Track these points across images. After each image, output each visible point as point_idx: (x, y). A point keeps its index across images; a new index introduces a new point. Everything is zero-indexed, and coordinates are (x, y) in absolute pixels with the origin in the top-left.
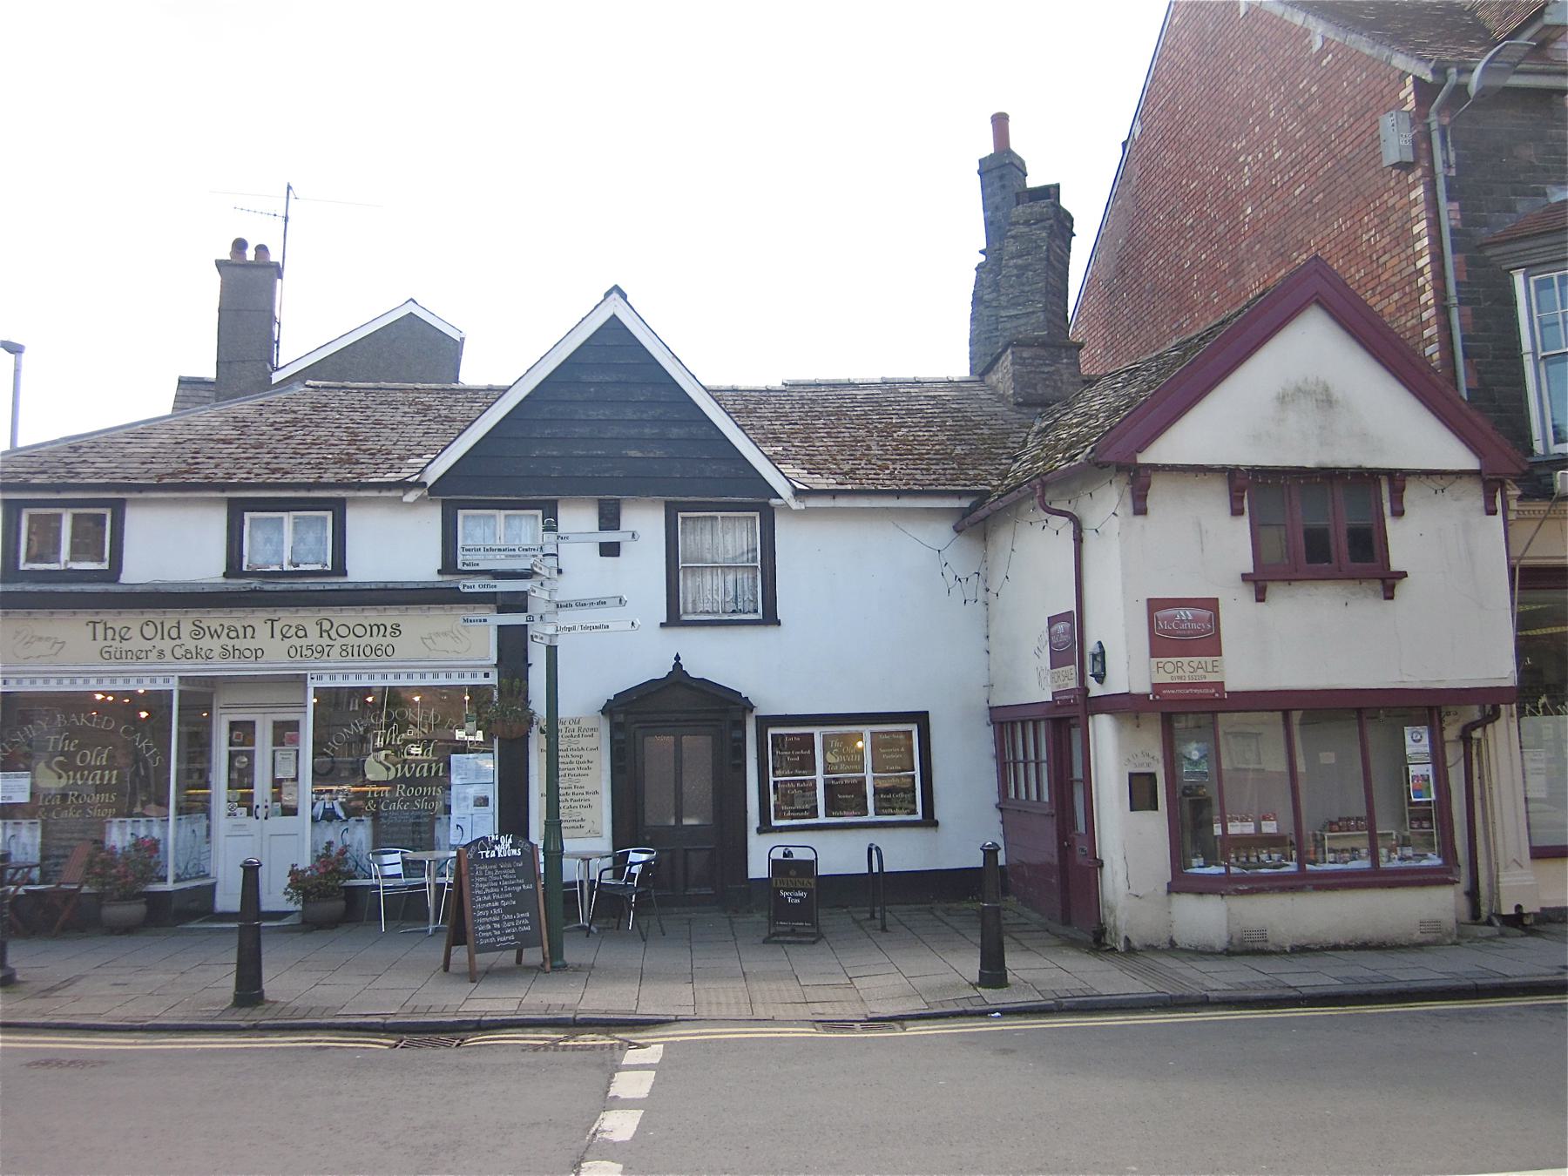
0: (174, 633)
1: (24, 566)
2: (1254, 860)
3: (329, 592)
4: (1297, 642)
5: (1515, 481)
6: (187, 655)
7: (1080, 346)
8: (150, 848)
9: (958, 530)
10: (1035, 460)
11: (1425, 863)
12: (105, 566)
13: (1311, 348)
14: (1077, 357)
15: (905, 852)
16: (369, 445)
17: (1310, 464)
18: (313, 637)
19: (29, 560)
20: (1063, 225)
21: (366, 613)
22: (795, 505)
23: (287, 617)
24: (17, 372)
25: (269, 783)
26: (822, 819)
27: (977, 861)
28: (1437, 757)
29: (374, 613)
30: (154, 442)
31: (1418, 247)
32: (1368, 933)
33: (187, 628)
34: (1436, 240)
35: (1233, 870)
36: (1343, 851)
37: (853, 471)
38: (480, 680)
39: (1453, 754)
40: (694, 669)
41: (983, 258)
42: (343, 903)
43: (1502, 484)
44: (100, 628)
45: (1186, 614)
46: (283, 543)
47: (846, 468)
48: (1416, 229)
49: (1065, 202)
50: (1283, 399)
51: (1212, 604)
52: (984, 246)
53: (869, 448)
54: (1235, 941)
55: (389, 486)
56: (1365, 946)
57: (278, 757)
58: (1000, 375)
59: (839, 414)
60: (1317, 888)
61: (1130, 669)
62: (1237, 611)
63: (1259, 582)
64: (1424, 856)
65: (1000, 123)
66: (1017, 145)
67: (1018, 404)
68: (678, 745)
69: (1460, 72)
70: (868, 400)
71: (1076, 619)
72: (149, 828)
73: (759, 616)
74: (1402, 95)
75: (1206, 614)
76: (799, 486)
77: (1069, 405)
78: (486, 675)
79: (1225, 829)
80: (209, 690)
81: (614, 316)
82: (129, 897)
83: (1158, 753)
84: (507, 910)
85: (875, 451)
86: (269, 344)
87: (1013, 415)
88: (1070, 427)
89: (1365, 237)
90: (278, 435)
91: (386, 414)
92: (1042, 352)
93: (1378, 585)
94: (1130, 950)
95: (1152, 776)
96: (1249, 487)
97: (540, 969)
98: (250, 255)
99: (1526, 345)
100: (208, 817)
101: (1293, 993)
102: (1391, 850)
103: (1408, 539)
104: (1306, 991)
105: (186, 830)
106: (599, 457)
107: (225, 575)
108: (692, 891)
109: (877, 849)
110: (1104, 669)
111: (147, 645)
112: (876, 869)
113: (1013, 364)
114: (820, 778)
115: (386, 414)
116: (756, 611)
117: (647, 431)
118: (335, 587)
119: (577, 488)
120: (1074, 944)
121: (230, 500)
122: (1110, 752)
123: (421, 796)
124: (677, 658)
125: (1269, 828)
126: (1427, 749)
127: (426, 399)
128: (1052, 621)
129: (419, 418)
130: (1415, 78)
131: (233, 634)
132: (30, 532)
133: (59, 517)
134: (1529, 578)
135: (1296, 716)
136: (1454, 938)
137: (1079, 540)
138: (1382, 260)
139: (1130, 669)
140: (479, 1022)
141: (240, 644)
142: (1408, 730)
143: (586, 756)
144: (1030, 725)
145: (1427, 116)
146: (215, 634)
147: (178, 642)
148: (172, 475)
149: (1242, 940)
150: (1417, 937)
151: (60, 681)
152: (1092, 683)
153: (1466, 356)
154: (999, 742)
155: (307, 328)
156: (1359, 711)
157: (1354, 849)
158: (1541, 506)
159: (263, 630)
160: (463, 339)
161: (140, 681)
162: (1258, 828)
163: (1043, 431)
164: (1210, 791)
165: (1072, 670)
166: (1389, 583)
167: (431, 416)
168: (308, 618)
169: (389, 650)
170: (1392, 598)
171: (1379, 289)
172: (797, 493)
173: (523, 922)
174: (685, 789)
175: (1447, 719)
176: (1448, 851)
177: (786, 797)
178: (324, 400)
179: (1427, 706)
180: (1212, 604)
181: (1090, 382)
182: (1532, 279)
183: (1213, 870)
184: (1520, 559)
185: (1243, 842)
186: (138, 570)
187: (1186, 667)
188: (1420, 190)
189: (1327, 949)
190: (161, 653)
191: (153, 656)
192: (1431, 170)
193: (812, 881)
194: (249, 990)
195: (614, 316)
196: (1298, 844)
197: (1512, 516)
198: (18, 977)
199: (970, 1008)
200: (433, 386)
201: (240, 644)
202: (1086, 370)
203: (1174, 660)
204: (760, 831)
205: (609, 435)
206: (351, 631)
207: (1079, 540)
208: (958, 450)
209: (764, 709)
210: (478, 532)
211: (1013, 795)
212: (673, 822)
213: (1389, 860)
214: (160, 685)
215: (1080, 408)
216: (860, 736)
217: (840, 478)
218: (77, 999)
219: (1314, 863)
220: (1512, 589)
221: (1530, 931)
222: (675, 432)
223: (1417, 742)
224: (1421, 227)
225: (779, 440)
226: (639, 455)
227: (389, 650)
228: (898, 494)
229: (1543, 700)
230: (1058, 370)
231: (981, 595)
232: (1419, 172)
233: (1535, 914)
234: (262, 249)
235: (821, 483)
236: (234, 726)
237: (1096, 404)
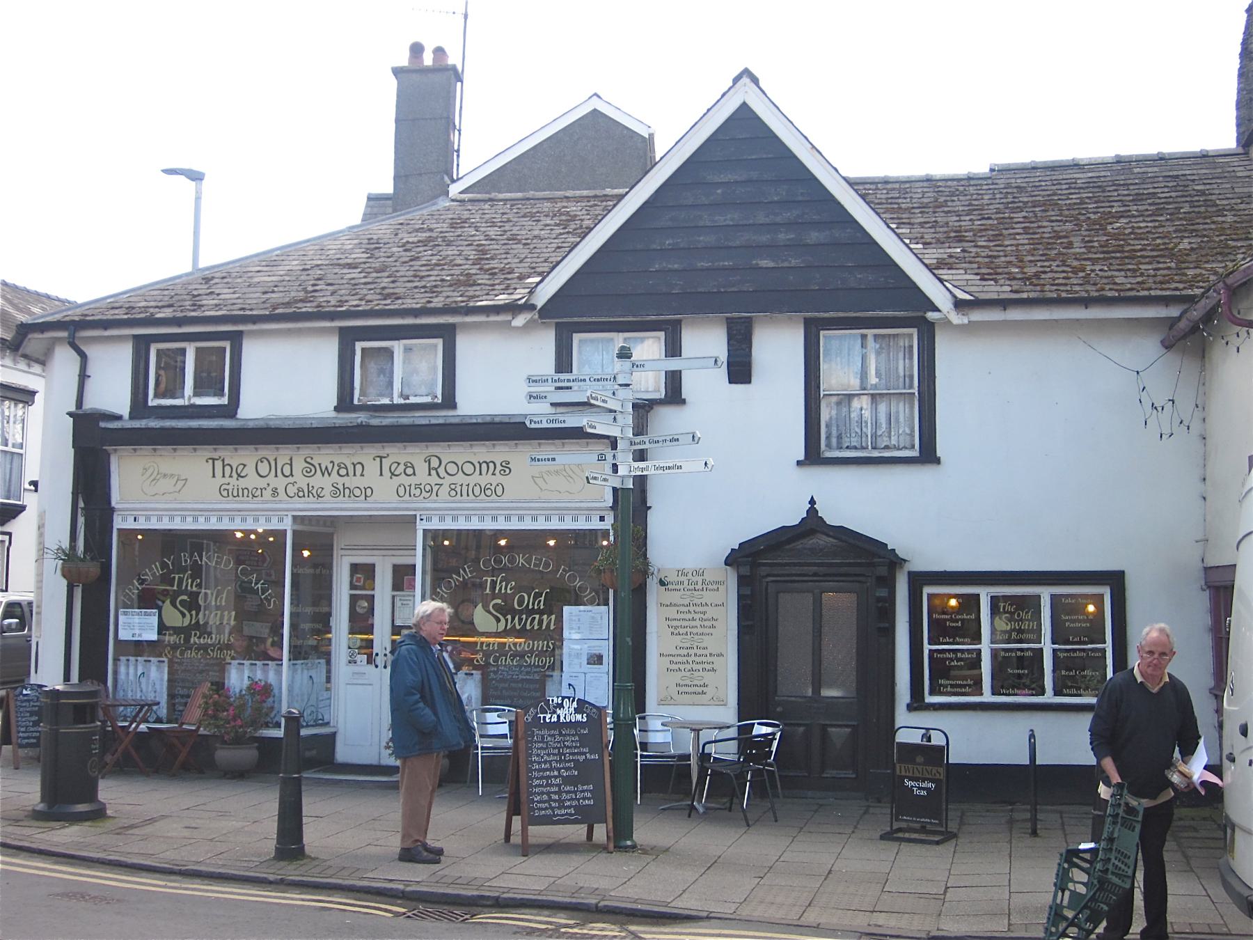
0: (287, 470)
1: (152, 402)
3: (439, 428)
6: (300, 493)
8: (262, 692)
9: (1168, 345)
12: (225, 400)
16: (494, 264)
18: (422, 476)
19: (156, 396)
21: (475, 450)
22: (956, 319)
23: (397, 453)
24: (198, 199)
25: (388, 628)
29: (484, 450)
30: (281, 270)
33: (299, 464)
38: (595, 524)
40: (832, 515)
44: (219, 464)
46: (412, 372)
47: (1031, 270)
53: (1070, 245)
55: (497, 310)
57: (398, 603)
59: (1048, 204)
68: (818, 603)
70: (1090, 184)
72: (265, 672)
73: (915, 453)
78: (602, 519)
80: (330, 530)
81: (744, 105)
82: (238, 741)
84: (568, 780)
85: (1078, 248)
86: (446, 155)
90: (406, 256)
91: (526, 229)
97: (604, 848)
98: (428, 59)
100: (328, 663)
105: (302, 677)
106: (725, 269)
107: (337, 409)
108: (830, 773)
111: (262, 483)
114: (985, 647)
115: (526, 229)
116: (913, 447)
117: (781, 236)
118: (441, 421)
119: (703, 304)
121: (341, 329)
123: (532, 651)
124: (812, 502)
127: (573, 208)
129: (558, 230)
131: (343, 472)
132: (158, 367)
133: (183, 352)
140: (497, 898)
141: (351, 482)
143: (711, 612)
146: (326, 472)
147: (291, 479)
148: (288, 304)
151: (184, 518)
155: (489, 135)
159: (372, 467)
160: (651, 136)
161: (256, 520)
167: (572, 226)
168: (416, 454)
169: (401, 492)
172: (959, 305)
173: (585, 795)
174: (824, 653)
177: (941, 668)
178: (466, 215)
186: (257, 404)
190: (275, 491)
191: (268, 494)
194: (290, 840)
195: (744, 105)
198: (109, 812)
200: (585, 193)
201: (351, 482)
204: (910, 708)
205: (738, 243)
206: (460, 469)
209: (922, 562)
210: (596, 358)
212: (810, 693)
214: (275, 525)
217: (1016, 285)
218: (145, 838)
222: (814, 236)
225: (960, 239)
226: (771, 264)
227: (401, 492)
228: (1086, 302)
234: (439, 51)
235: (992, 290)
236: (355, 568)
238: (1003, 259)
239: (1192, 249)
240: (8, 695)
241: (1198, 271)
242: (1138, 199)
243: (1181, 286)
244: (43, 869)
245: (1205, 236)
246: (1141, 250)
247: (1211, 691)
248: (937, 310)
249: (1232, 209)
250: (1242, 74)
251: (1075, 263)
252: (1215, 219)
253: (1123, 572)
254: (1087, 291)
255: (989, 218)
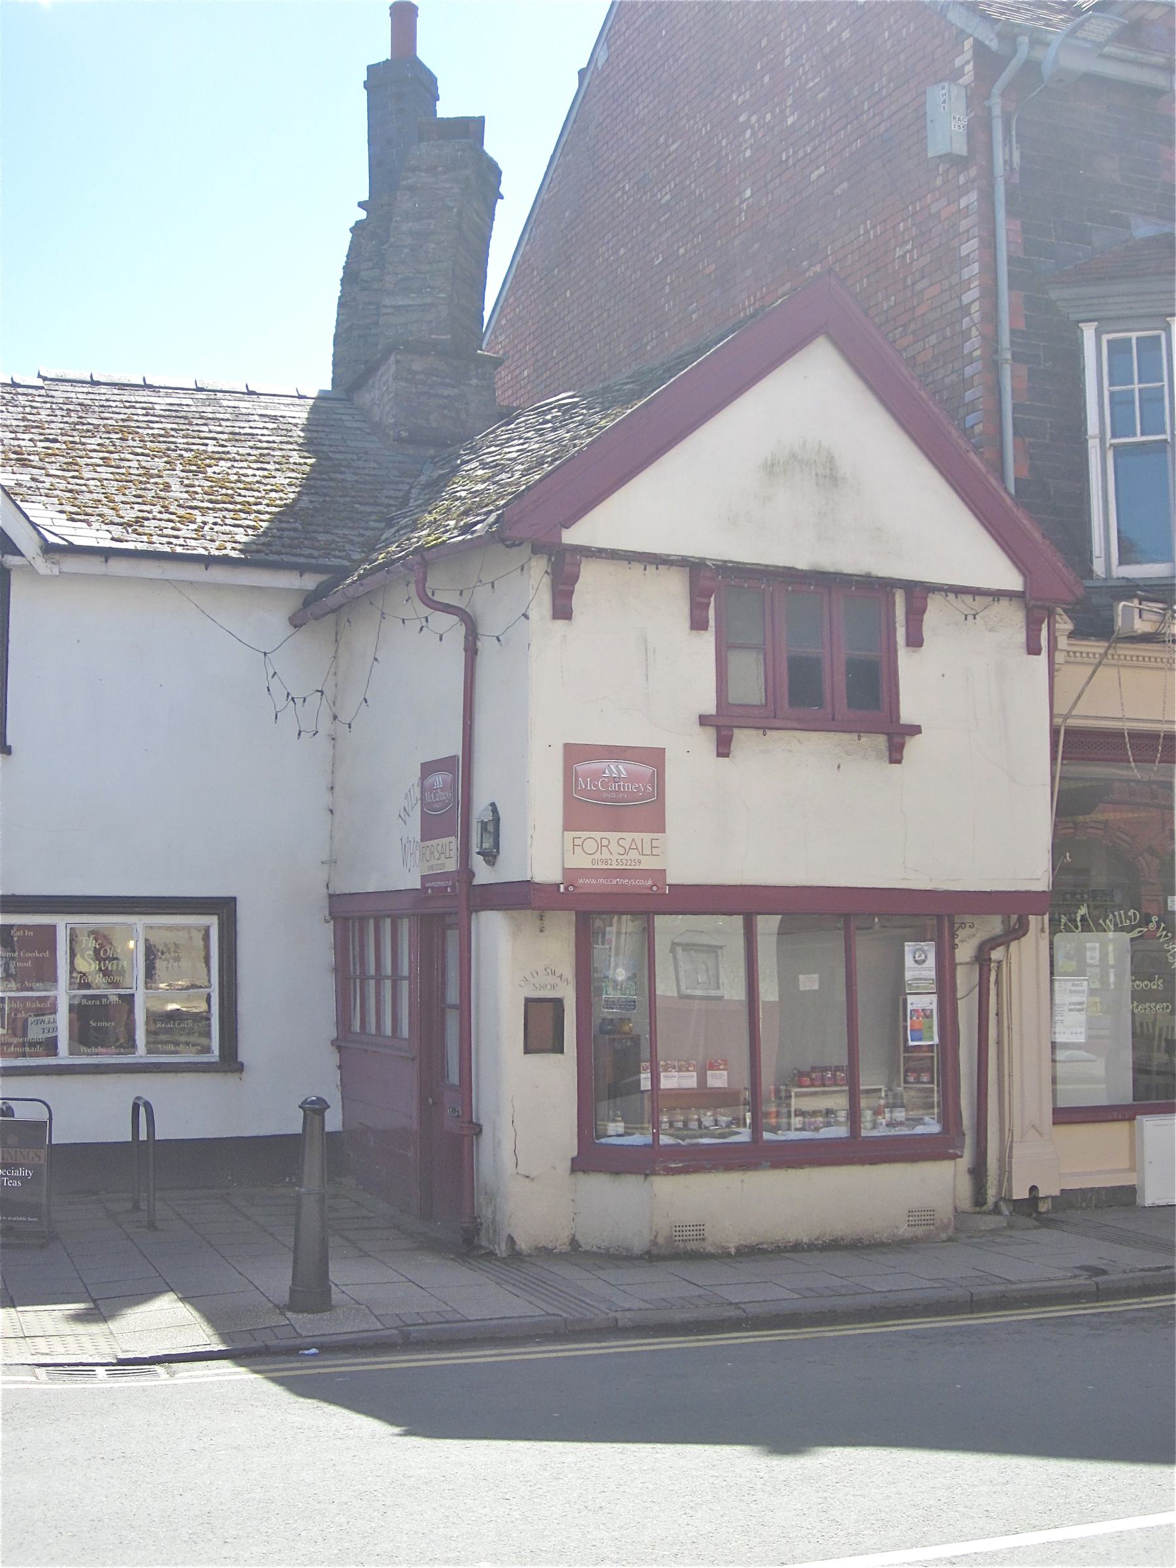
2: (694, 1125)
4: (777, 815)
5: (1065, 611)
11: (919, 1130)
13: (812, 399)
15: (190, 1109)
17: (802, 564)
20: (486, 180)
22: (42, 566)
26: (64, 1055)
27: (295, 1126)
28: (945, 985)
31: (966, 274)
32: (841, 1226)
34: (990, 267)
35: (665, 1140)
36: (814, 1113)
37: (139, 521)
39: (965, 979)
41: (362, 215)
43: (1051, 614)
45: (617, 769)
47: (130, 514)
48: (965, 250)
49: (492, 146)
50: (772, 468)
51: (655, 757)
54: (660, 1240)
56: (834, 1245)
59: (125, 430)
60: (776, 1165)
61: (542, 847)
62: (690, 763)
63: (723, 728)
64: (920, 1121)
65: (404, 20)
66: (426, 52)
69: (1033, 43)
70: (173, 413)
71: (460, 768)
74: (958, 62)
75: (647, 770)
76: (52, 539)
79: (655, 1080)
83: (567, 968)
85: (177, 491)
89: (899, 252)
93: (881, 741)
94: (515, 1255)
95: (558, 1003)
96: (715, 588)
99: (1093, 427)
101: (733, 1313)
102: (877, 1112)
103: (923, 682)
104: (753, 1310)
109: (147, 1105)
110: (497, 844)
112: (143, 1137)
114: (63, 995)
120: (435, 1246)
122: (513, 965)
125: (718, 1080)
126: (932, 974)
128: (428, 769)
130: (975, 40)
134: (1074, 744)
135: (768, 925)
136: (950, 1232)
137: (471, 652)
138: (919, 287)
139: (542, 847)
142: (909, 947)
144: (387, 924)
145: (988, 97)
149: (670, 1239)
150: (904, 1231)
152: (478, 863)
153: (1015, 434)
154: (341, 946)
156: (846, 917)
157: (829, 1112)
158: (1096, 647)
162: (702, 1080)
164: (638, 1023)
165: (452, 843)
166: (897, 739)
170: (899, 761)
171: (912, 327)
172: (48, 549)
175: (961, 934)
176: (949, 1115)
179: (933, 913)
180: (655, 757)
182: (1105, 338)
183: (637, 1139)
184: (1066, 717)
185: (683, 1099)
187: (614, 847)
188: (973, 196)
189: (786, 1249)
192: (988, 173)
193: (43, 1153)
196: (755, 1104)
197: (1059, 657)
199: (272, 1342)
203: (597, 835)
207: (471, 652)
211: (357, 1026)
213: (875, 1126)
216: (130, 932)
217: (117, 531)
219: (774, 1129)
220: (1054, 758)
221: (1046, 1222)
223: (919, 963)
224: (970, 247)
225: (24, 463)
229: (1083, 911)
231: (325, 725)
232: (973, 172)
233: (1054, 1198)
238: (88, 496)
239: (315, 509)
240: (869, 1108)
241: (330, 537)
242: (235, 437)
243: (316, 553)
244: (788, 1334)
245: (325, 495)
246: (256, 504)
247: (333, 1043)
248: (19, 553)
249: (349, 466)
250: (342, 304)
251: (181, 512)
252: (334, 476)
253: (235, 899)
254: (205, 548)
255: (55, 441)
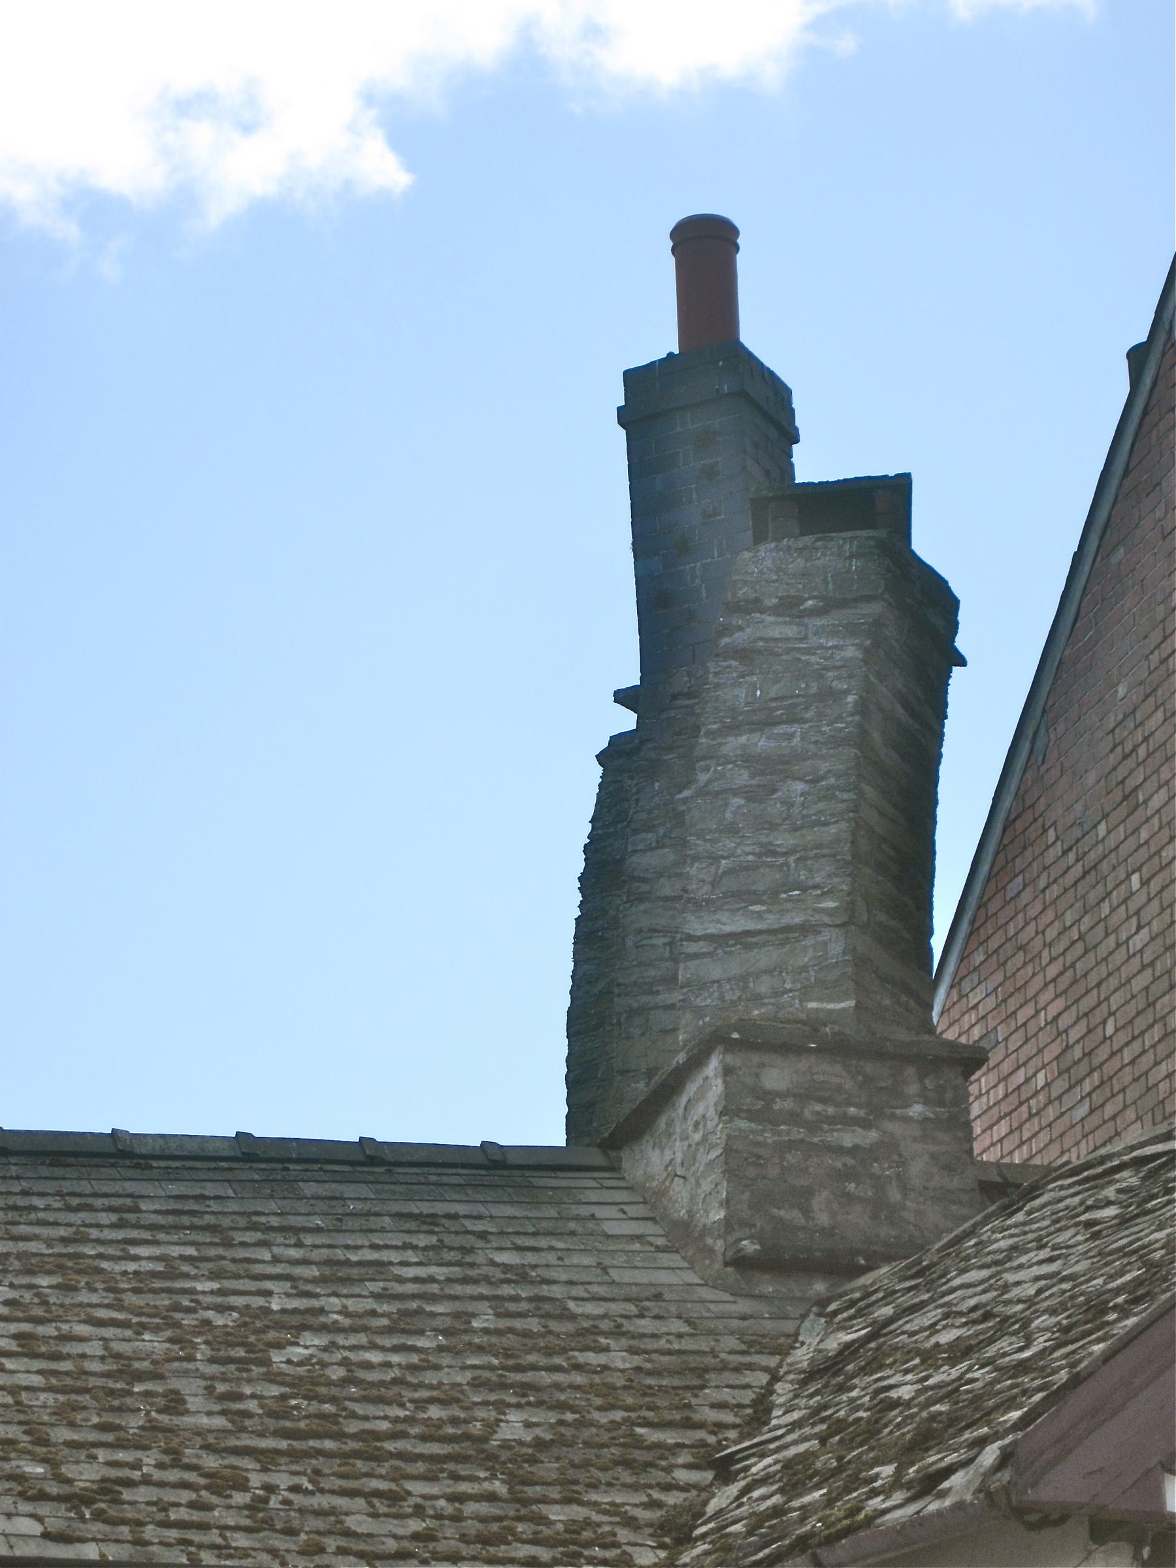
7: (971, 1060)
10: (795, 1477)
14: (961, 1101)
20: (923, 622)
37: (108, 1489)
41: (627, 720)
42: (850, 1145)
47: (85, 1475)
49: (927, 542)
52: (632, 677)
53: (175, 1403)
58: (677, 1150)
65: (705, 252)
67: (741, 1262)
77: (926, 1276)
85: (200, 1415)
87: (719, 1303)
88: (930, 1358)
92: (832, 1073)
113: (728, 1111)
163: (828, 1370)
181: (1005, 1191)
202: (991, 1145)
208: (514, 1427)
215: (967, 1285)
217: (57, 1517)
230: (889, 1146)
237: (1025, 1278)
